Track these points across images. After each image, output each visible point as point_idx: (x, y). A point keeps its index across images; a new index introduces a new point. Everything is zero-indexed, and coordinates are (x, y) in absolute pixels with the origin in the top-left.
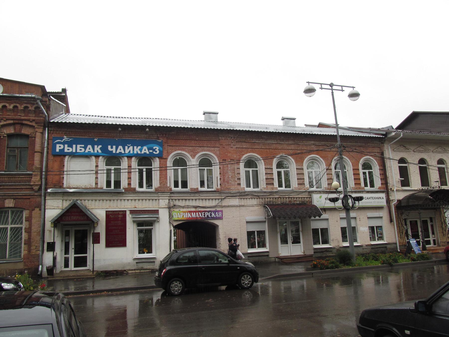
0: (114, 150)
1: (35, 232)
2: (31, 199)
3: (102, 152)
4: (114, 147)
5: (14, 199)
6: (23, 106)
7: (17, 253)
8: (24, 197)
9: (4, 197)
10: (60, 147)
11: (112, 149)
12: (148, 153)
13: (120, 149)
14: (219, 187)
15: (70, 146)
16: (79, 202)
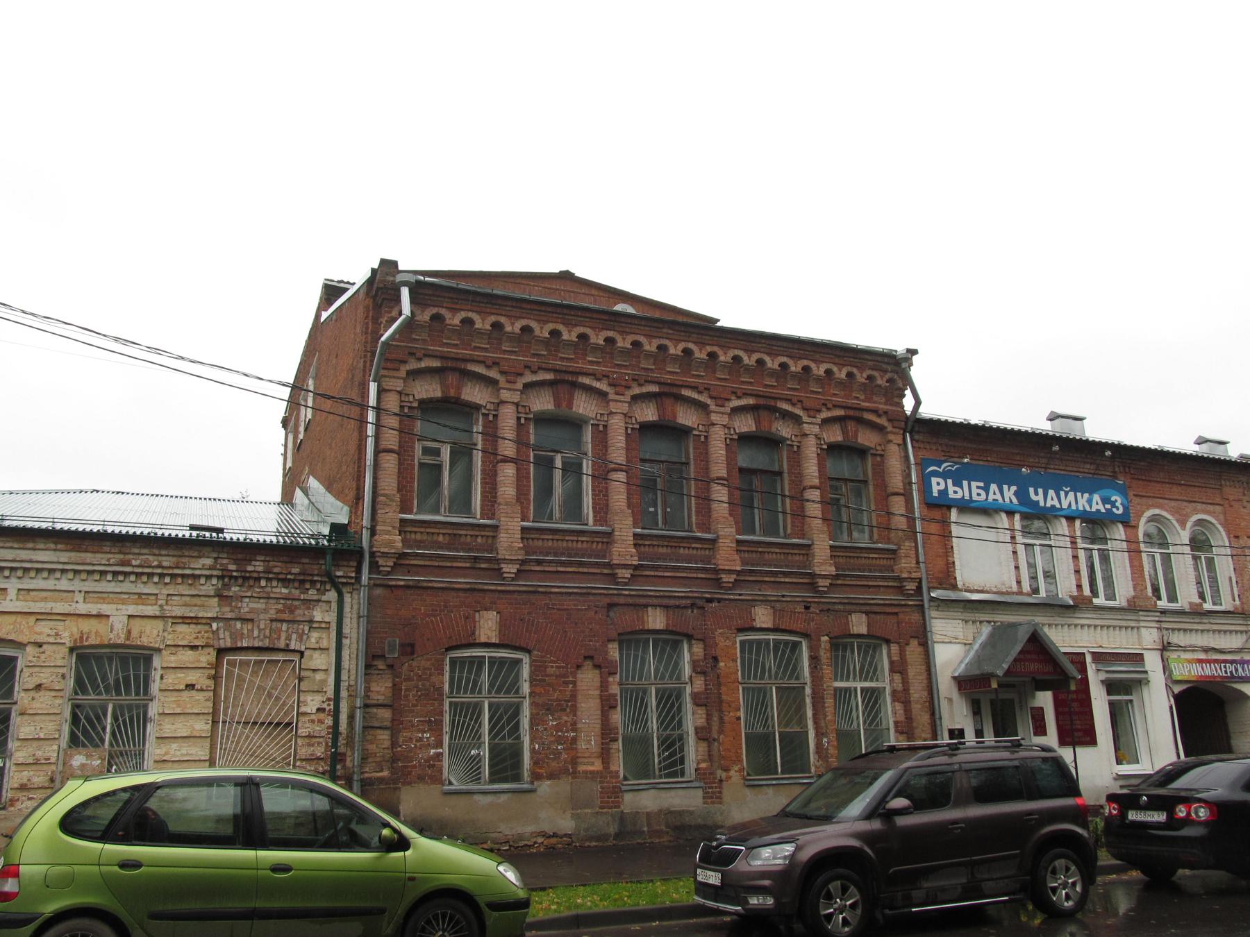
0: (1040, 498)
1: (917, 702)
2: (901, 616)
3: (1020, 503)
4: (1040, 491)
5: (867, 613)
6: (865, 375)
7: (674, 764)
8: (888, 610)
9: (848, 607)
10: (938, 484)
11: (1037, 496)
12: (1103, 511)
13: (1052, 501)
14: (1237, 602)
15: (958, 483)
16: (1046, 629)
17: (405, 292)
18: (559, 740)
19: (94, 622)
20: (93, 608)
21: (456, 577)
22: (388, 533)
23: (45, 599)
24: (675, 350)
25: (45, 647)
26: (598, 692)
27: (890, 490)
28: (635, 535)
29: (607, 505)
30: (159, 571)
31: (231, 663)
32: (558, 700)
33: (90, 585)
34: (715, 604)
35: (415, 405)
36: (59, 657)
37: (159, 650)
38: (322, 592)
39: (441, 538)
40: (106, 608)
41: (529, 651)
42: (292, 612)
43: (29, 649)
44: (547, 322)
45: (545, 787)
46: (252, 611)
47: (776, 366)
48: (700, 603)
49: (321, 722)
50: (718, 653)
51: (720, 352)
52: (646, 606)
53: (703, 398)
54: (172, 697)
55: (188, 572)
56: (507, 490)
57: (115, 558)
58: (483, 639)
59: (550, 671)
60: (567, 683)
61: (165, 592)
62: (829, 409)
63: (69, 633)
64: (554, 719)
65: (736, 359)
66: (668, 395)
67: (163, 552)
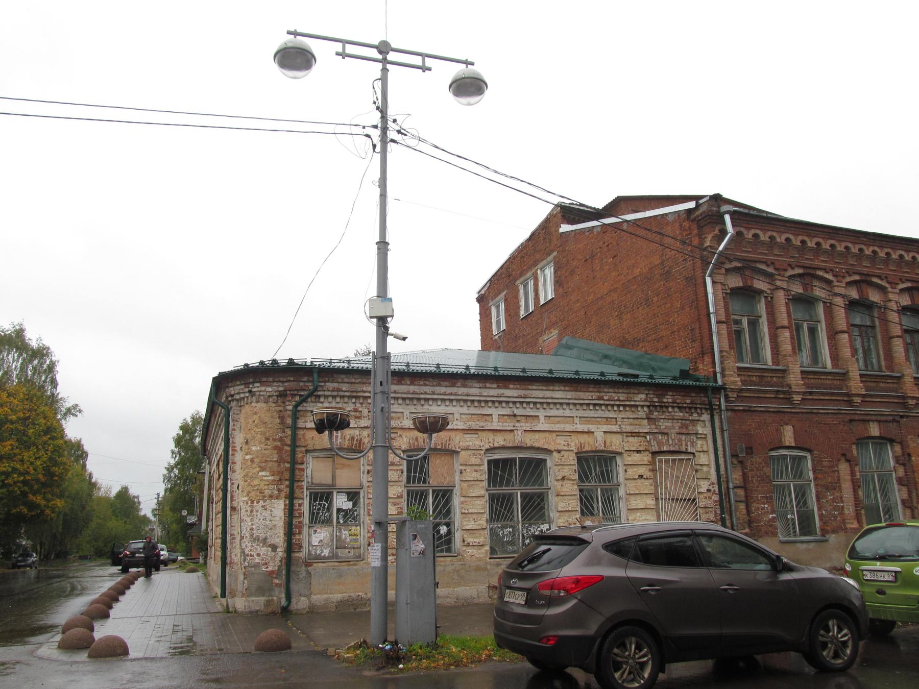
17: (727, 218)
18: (835, 508)
19: (586, 436)
20: (585, 427)
21: (768, 403)
22: (732, 376)
23: (558, 422)
24: (868, 252)
25: (563, 453)
26: (849, 477)
27: (778, 325)
28: (861, 375)
29: (837, 355)
30: (618, 403)
31: (660, 461)
32: (831, 482)
33: (581, 413)
34: (904, 420)
35: (729, 291)
36: (572, 459)
37: (620, 454)
38: (700, 415)
39: (754, 379)
40: (592, 428)
41: (809, 450)
42: (687, 428)
43: (555, 454)
44: (799, 235)
45: (832, 538)
46: (667, 427)
47: (910, 259)
48: (897, 418)
49: (710, 498)
50: (911, 451)
51: (892, 253)
52: (869, 421)
53: (884, 283)
54: (631, 484)
55: (633, 403)
56: (846, 352)
57: (595, 395)
58: (787, 444)
59: (825, 464)
60: (834, 471)
61: (620, 416)
62: (793, 268)
63: (574, 443)
64: (833, 494)
65: (901, 256)
66: (864, 282)
67: (621, 391)
